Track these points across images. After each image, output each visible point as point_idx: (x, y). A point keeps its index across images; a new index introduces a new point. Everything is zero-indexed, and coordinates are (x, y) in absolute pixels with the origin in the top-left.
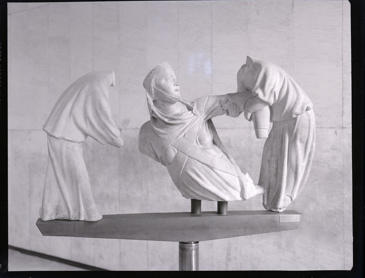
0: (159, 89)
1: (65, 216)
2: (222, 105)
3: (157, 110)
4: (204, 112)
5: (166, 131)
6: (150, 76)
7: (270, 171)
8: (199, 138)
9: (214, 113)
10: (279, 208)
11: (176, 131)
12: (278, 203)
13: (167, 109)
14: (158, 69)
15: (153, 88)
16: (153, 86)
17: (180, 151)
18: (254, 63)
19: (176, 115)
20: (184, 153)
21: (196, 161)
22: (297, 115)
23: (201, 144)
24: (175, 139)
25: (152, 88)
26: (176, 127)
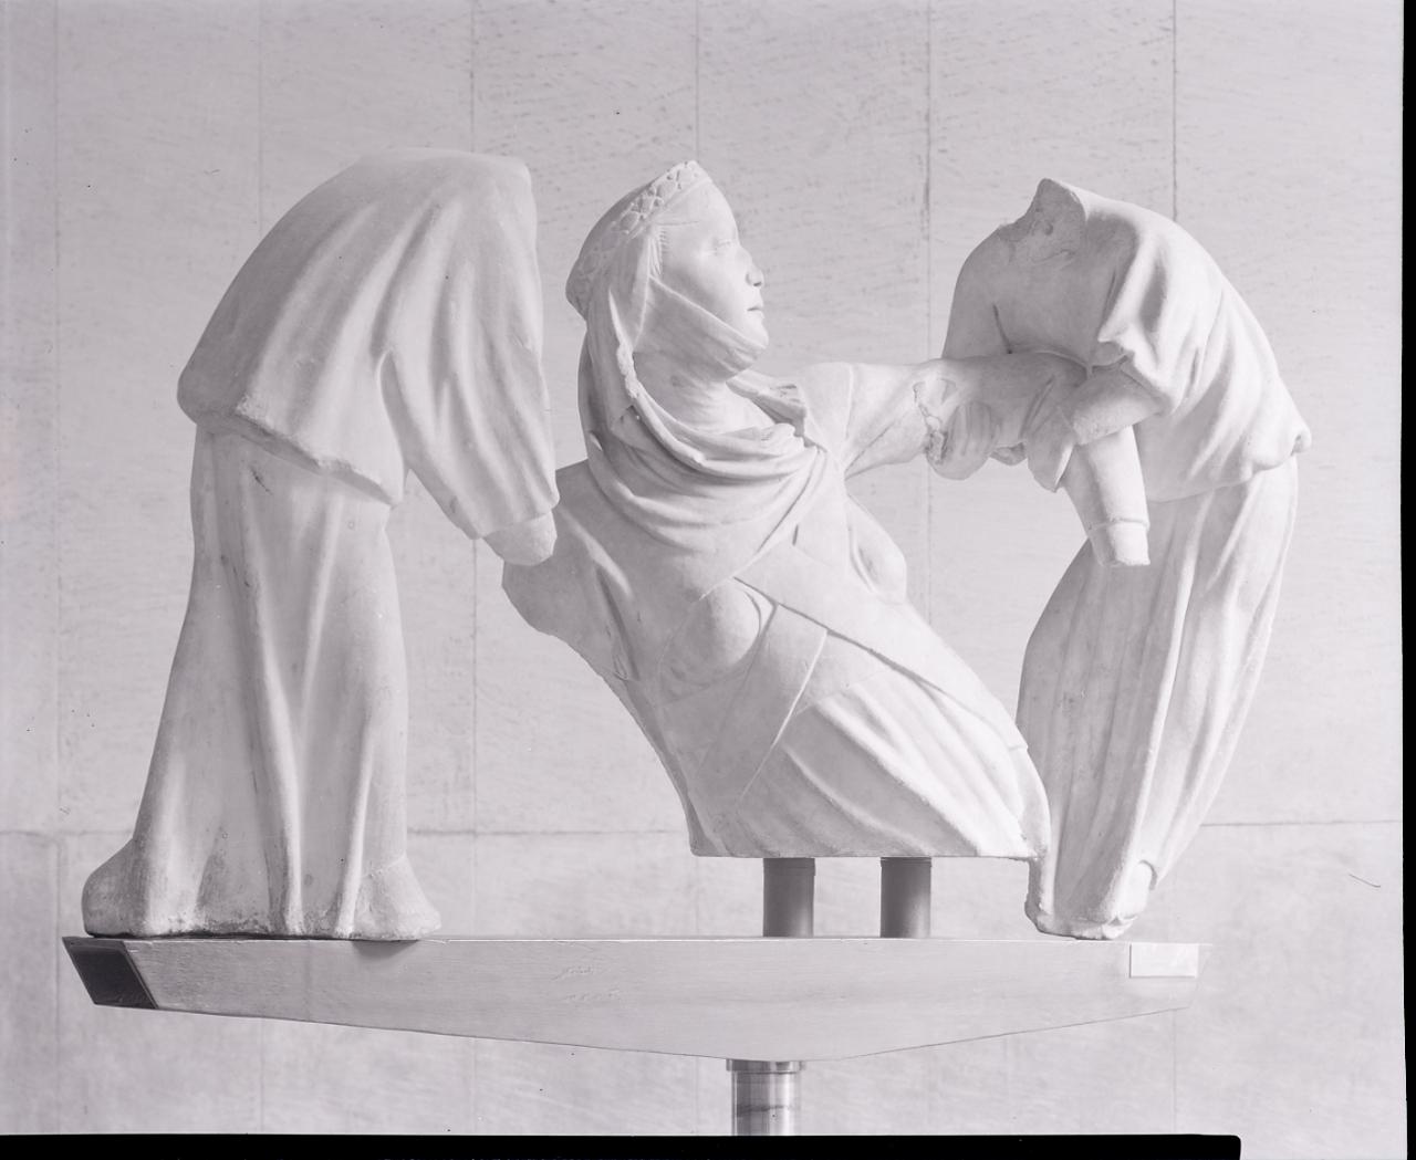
0: (681, 296)
1: (245, 912)
2: (926, 409)
3: (650, 403)
4: (847, 435)
6: (637, 221)
7: (1073, 750)
8: (861, 552)
10: (1113, 918)
12: (1111, 896)
13: (699, 405)
15: (647, 283)
16: (649, 275)
17: (783, 606)
18: (1087, 215)
19: (741, 435)
20: (806, 617)
21: (865, 653)
22: (1259, 467)
23: (875, 580)
26: (748, 495)
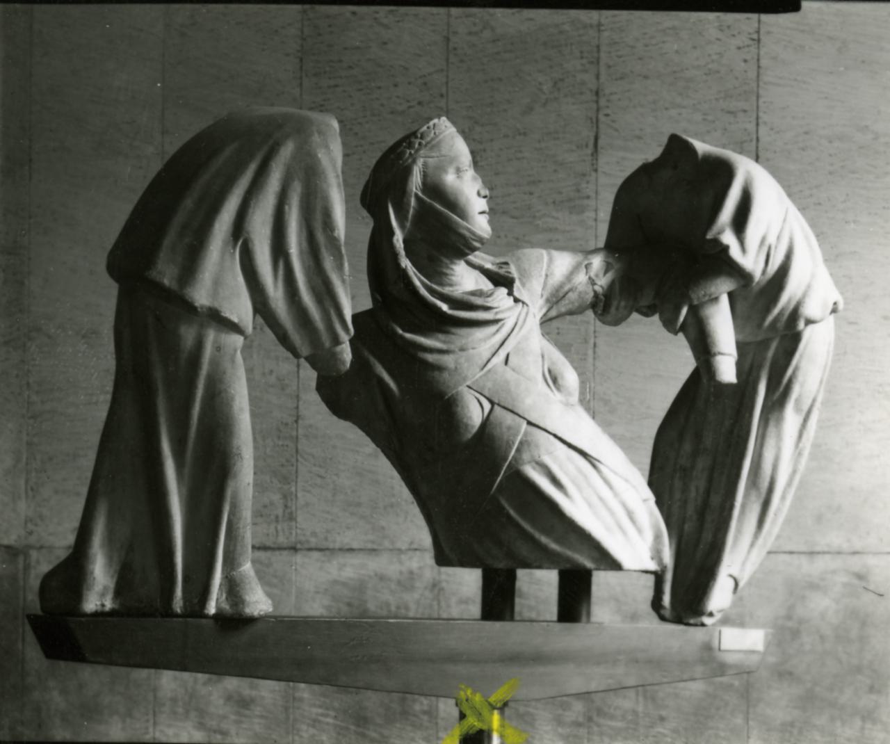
3: (414, 273)
4: (542, 296)
5: (444, 342)
6: (407, 155)
8: (550, 371)
9: (567, 302)
11: (481, 342)
14: (432, 135)
16: (414, 189)
17: (499, 405)
20: (512, 412)
21: (551, 438)
24: (478, 370)
25: (411, 196)
26: (479, 333)
